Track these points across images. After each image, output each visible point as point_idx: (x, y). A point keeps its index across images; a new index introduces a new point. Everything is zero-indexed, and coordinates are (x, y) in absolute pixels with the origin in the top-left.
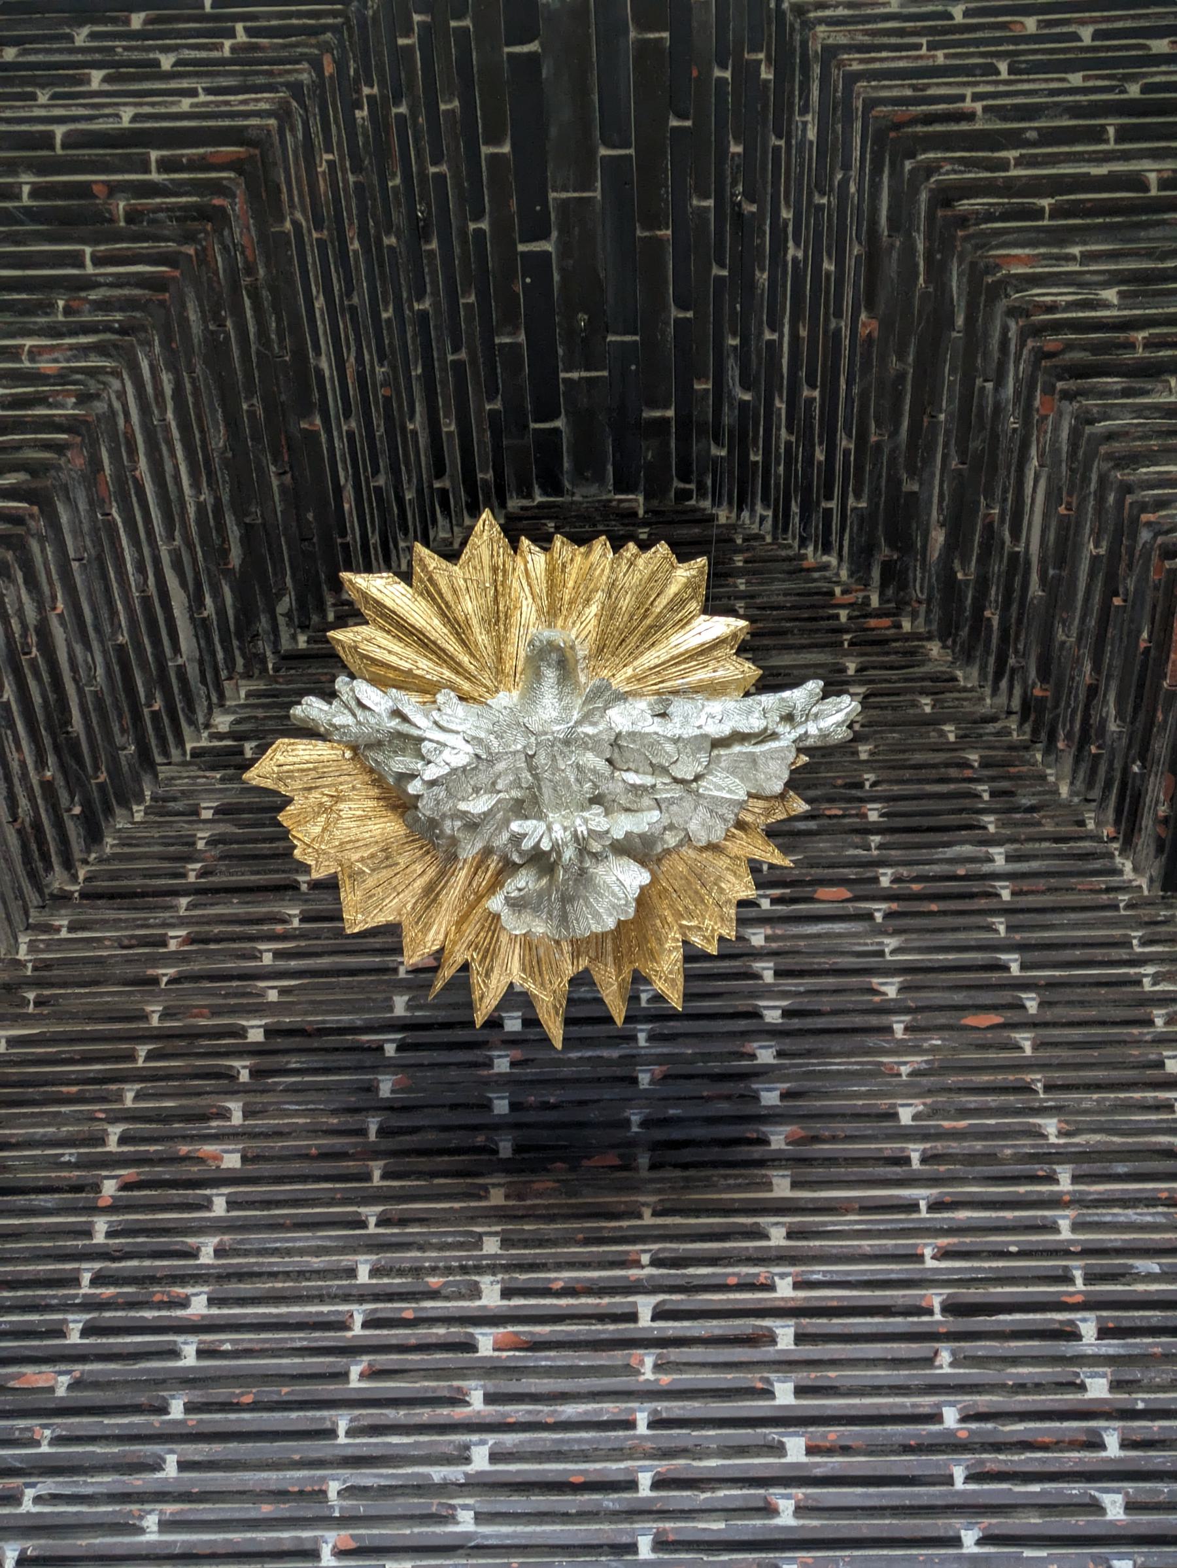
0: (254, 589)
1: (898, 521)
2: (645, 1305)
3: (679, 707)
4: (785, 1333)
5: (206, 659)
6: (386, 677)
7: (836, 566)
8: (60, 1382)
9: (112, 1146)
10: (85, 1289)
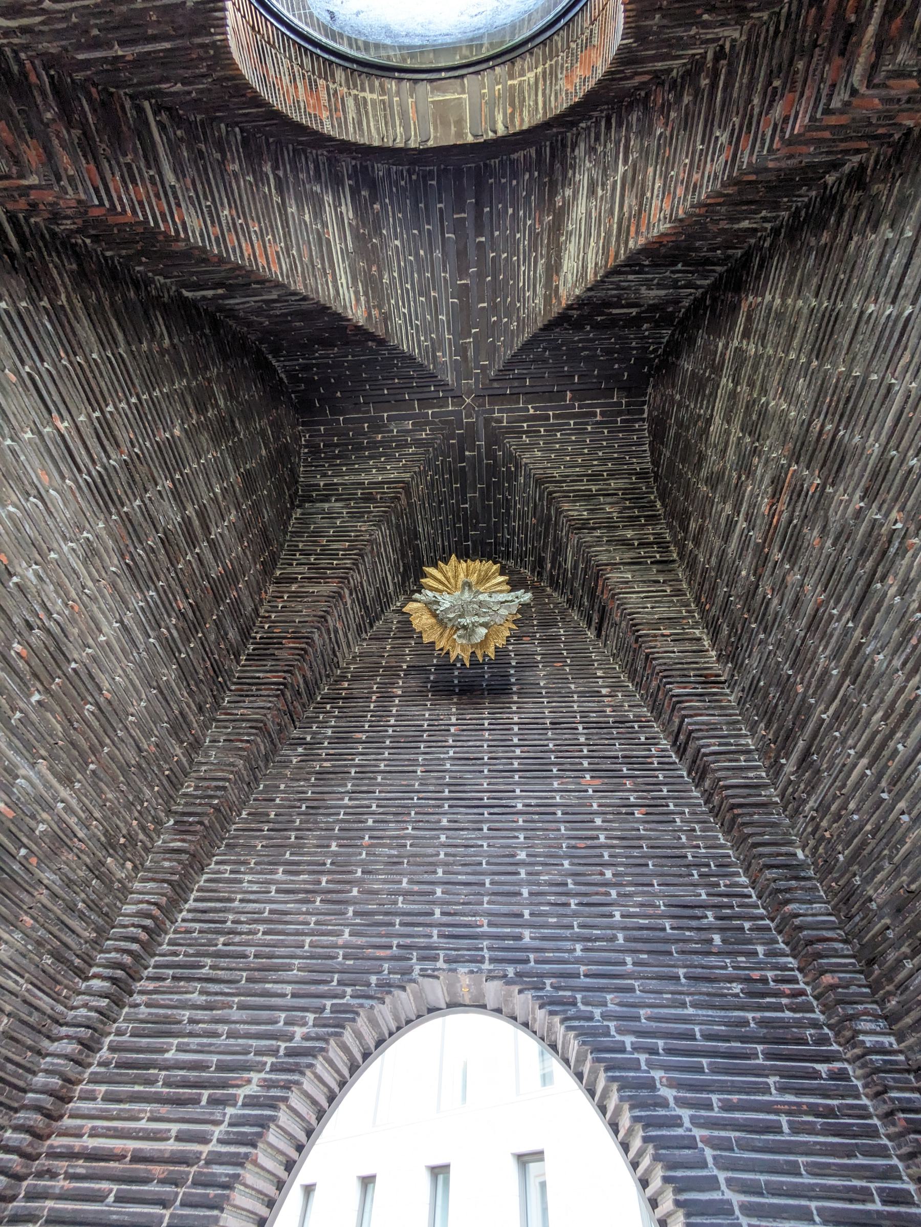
0: (405, 576)
1: (541, 562)
2: (486, 722)
4: (516, 728)
6: (432, 589)
7: (528, 573)
8: (363, 737)
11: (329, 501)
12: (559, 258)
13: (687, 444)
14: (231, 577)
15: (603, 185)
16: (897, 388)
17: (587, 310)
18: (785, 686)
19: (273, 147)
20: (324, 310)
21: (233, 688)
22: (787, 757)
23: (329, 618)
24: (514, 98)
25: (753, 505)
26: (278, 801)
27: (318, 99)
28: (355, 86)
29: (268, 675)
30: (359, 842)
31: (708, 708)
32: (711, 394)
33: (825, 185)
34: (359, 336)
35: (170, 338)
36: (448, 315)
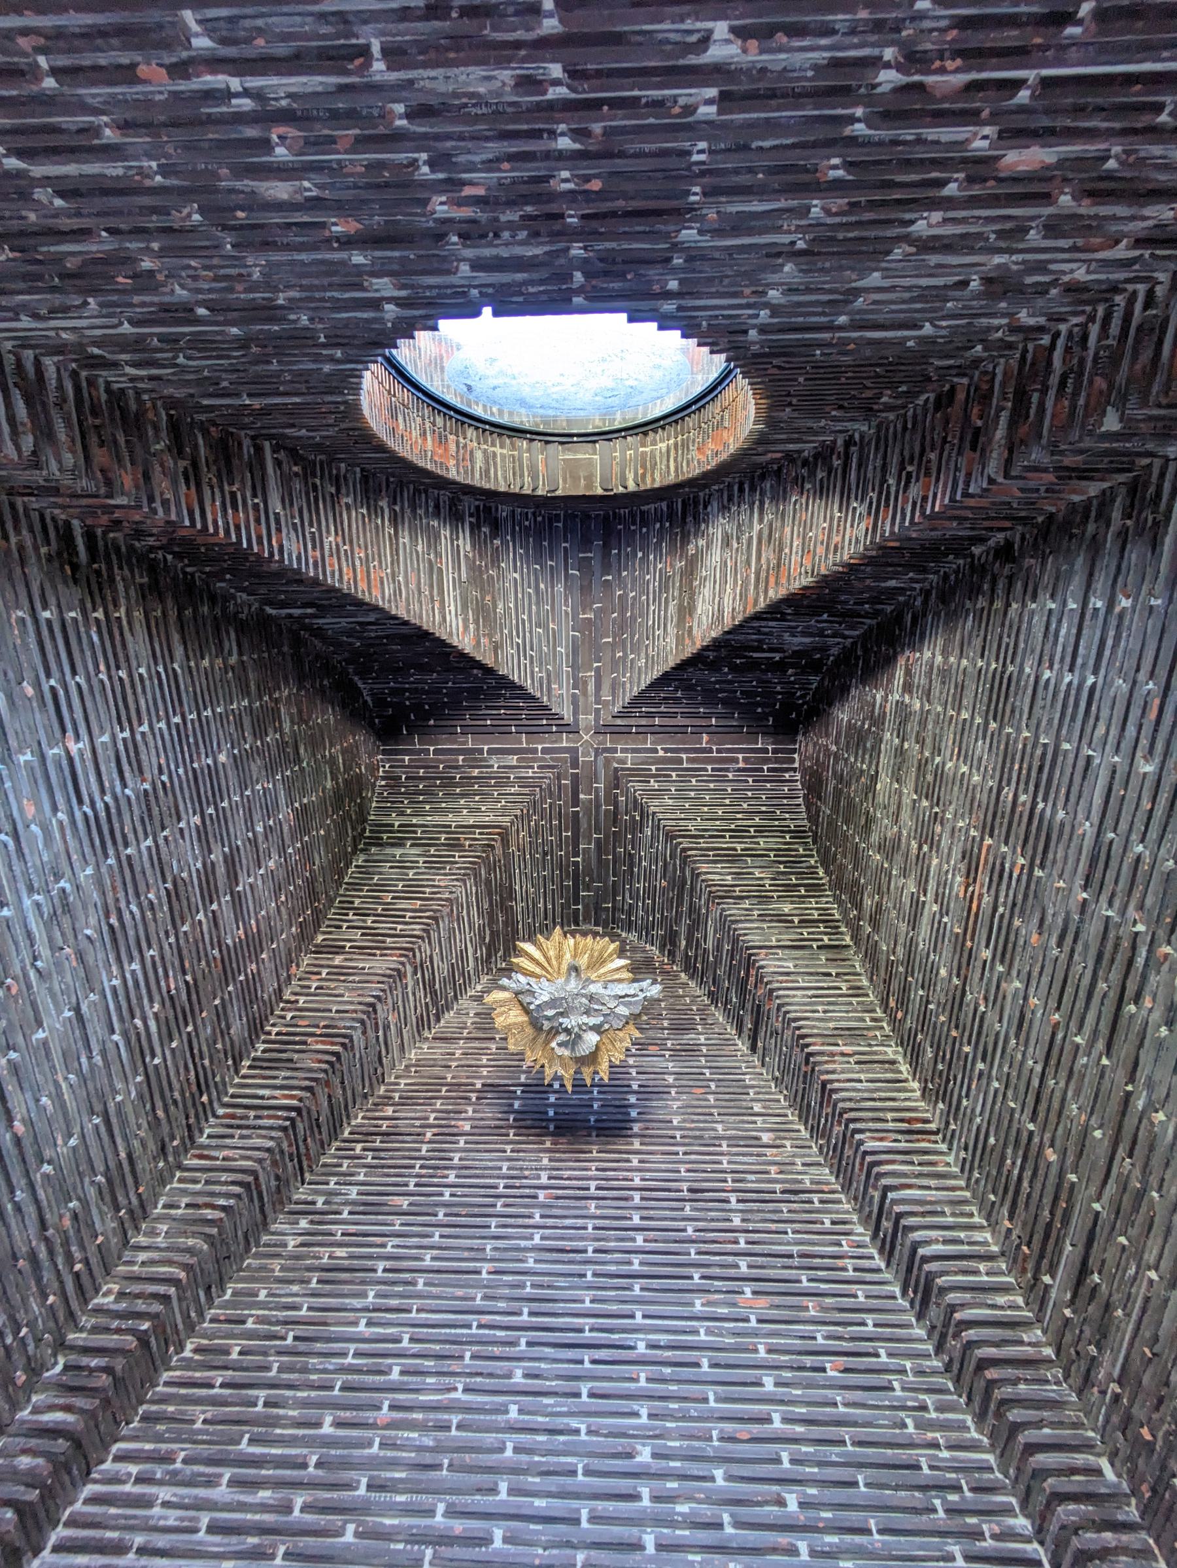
0: (491, 949)
2: (593, 1184)
3: (610, 985)
4: (637, 1196)
5: (476, 969)
6: (527, 973)
8: (404, 1202)
9: (431, 1121)
10: (417, 1170)
11: (402, 845)
12: (692, 599)
13: (851, 804)
14: (253, 945)
15: (738, 538)
16: (1097, 761)
17: (724, 652)
18: (1030, 1154)
19: (392, 486)
20: (424, 636)
21: (221, 1112)
22: (1052, 1273)
23: (379, 1007)
24: (643, 461)
25: (942, 884)
26: (250, 1324)
27: (446, 450)
28: (486, 442)
29: (277, 1093)
30: (370, 1415)
31: (920, 1175)
32: (873, 748)
33: (972, 556)
34: (467, 663)
35: (240, 654)
36: (567, 647)
